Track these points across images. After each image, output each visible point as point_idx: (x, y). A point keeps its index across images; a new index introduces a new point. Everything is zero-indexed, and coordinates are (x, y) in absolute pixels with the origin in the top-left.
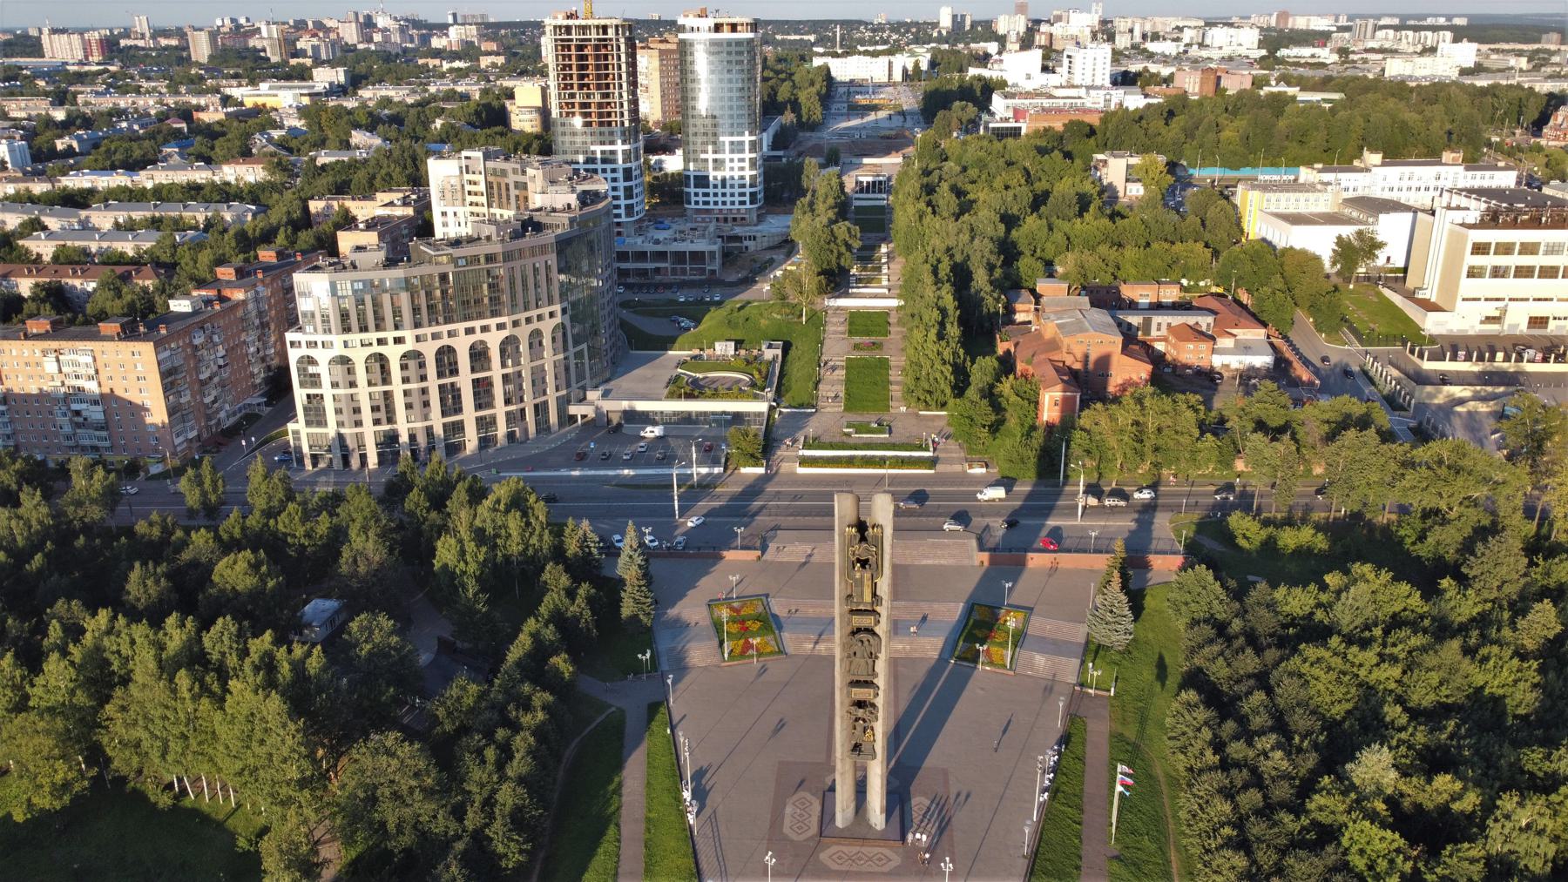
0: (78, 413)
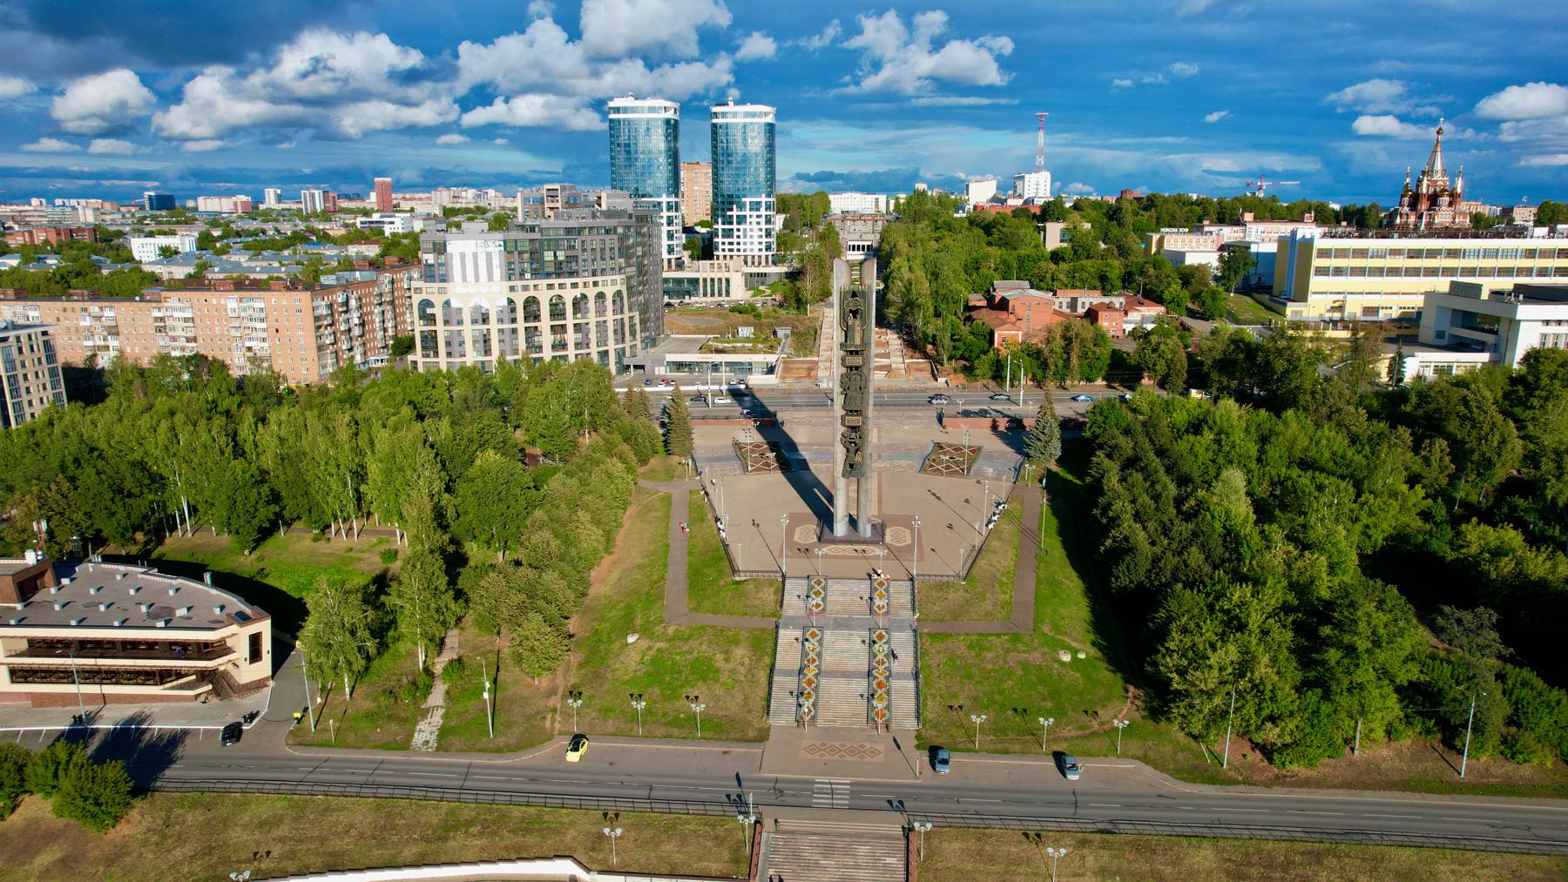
0: (250, 349)
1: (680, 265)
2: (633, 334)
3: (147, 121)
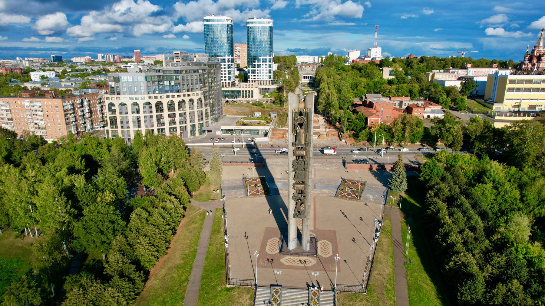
0: (36, 124)
1: (234, 84)
2: (207, 116)
3: (65, 31)
